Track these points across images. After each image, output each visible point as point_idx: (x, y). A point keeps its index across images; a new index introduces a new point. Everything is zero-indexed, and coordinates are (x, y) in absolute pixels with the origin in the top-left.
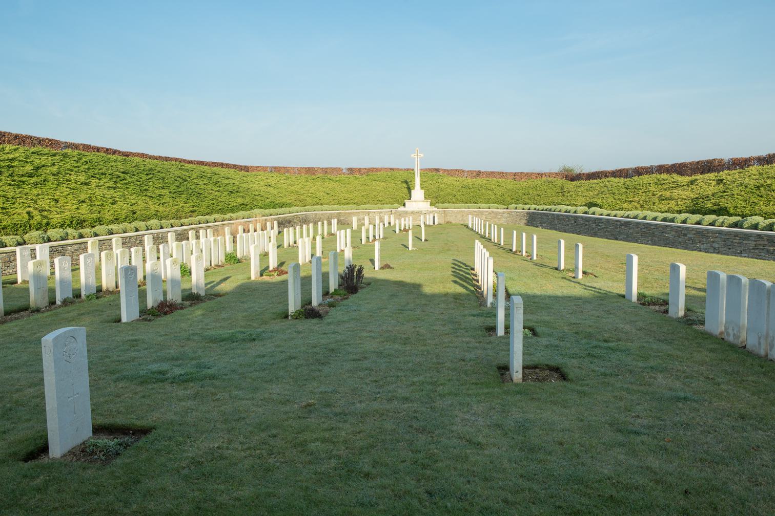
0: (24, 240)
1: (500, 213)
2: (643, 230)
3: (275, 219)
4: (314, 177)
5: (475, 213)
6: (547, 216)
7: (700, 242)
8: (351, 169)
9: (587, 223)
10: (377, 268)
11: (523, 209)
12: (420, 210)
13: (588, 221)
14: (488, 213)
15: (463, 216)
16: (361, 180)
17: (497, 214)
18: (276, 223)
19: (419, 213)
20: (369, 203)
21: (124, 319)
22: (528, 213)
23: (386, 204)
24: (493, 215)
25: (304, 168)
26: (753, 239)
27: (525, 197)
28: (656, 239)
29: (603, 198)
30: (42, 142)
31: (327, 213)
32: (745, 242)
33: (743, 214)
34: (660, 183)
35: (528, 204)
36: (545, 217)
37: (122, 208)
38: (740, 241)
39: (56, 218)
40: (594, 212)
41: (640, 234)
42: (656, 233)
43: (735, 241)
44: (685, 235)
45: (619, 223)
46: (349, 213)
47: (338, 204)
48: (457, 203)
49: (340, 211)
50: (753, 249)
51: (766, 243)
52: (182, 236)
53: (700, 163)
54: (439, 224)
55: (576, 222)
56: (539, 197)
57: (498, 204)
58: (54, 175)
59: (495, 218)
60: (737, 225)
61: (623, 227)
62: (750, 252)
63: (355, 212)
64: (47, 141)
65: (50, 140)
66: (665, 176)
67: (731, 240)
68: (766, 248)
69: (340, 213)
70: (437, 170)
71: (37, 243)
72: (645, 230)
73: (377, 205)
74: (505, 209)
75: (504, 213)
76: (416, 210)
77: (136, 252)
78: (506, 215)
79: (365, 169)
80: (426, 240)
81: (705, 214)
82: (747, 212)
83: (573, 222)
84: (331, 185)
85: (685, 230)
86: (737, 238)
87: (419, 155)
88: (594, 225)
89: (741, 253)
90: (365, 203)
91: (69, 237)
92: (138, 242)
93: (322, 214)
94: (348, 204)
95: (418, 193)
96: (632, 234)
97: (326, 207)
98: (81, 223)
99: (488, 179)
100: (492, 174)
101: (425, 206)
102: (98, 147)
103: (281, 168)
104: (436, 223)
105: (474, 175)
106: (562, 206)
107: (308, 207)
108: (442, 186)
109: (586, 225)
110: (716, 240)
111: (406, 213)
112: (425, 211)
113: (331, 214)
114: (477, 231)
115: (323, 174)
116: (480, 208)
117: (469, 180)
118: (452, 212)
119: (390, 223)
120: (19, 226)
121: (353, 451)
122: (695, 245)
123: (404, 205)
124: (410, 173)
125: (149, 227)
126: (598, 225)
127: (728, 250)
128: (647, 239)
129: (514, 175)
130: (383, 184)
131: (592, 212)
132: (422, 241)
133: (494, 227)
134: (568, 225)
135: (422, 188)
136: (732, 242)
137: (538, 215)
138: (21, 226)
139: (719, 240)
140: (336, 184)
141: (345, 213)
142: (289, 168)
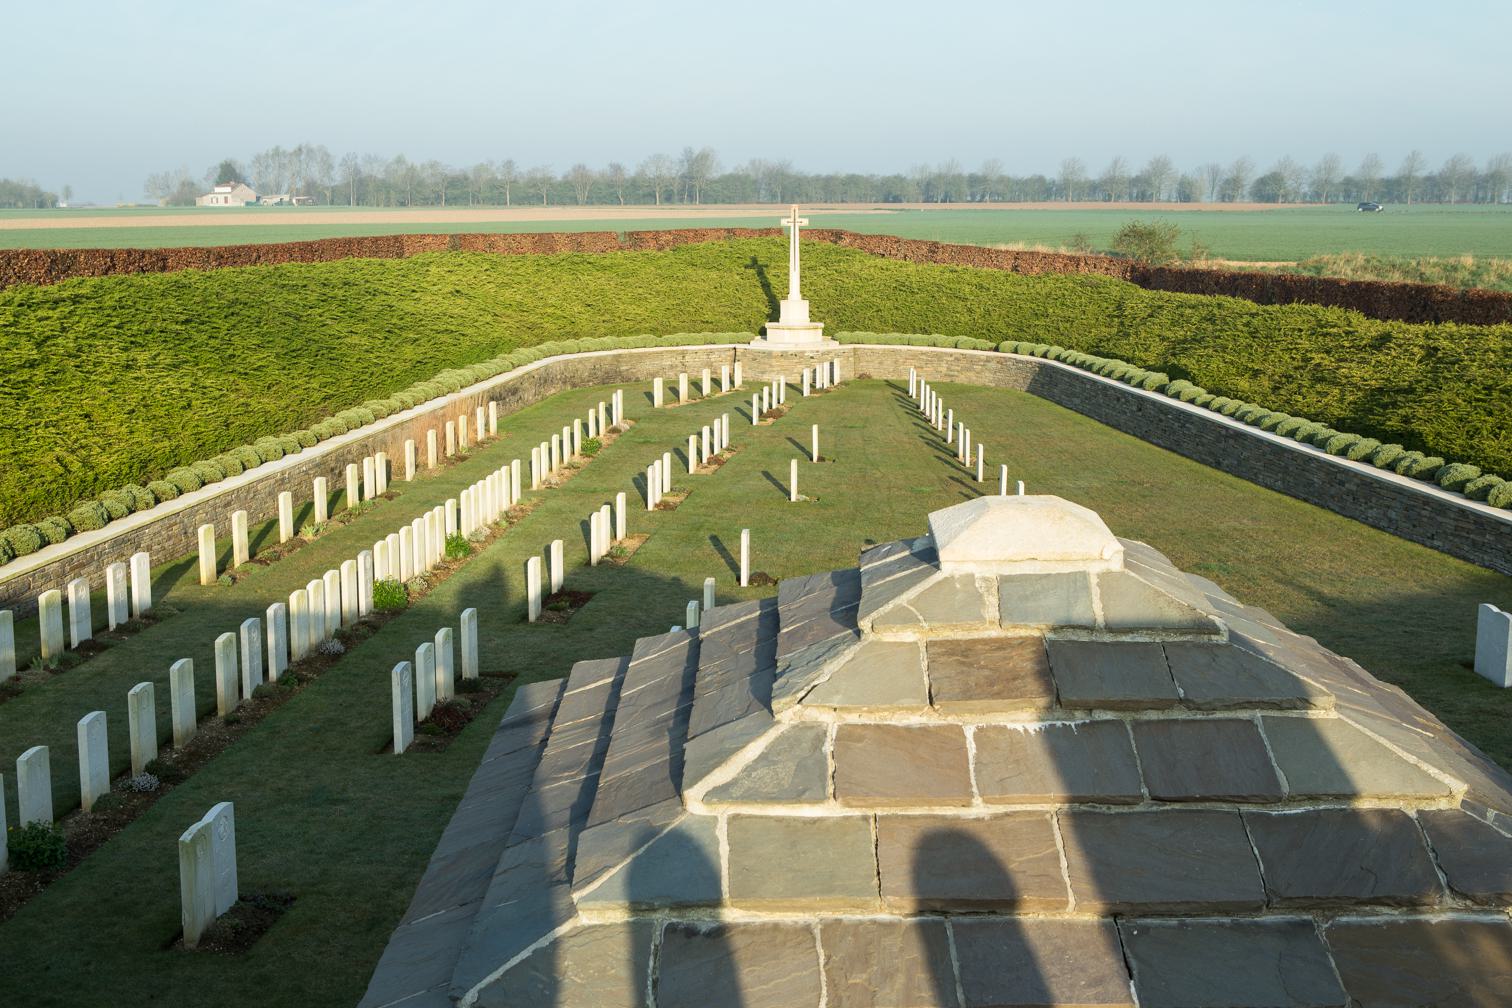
0: (71, 524)
1: (980, 360)
2: (1268, 456)
4: (552, 259)
5: (924, 357)
6: (1082, 382)
7: (1366, 503)
8: (638, 233)
9: (1162, 417)
10: (744, 582)
11: (1032, 354)
12: (799, 349)
13: (1166, 414)
14: (952, 359)
15: (896, 362)
16: (661, 262)
17: (972, 360)
20: (683, 329)
22: (1043, 367)
23: (722, 331)
24: (963, 363)
25: (528, 235)
26: (1452, 516)
27: (1037, 322)
28: (1291, 480)
29: (1202, 356)
30: (13, 261)
32: (1440, 519)
33: (1448, 452)
34: (1319, 329)
35: (1044, 341)
36: (1077, 383)
37: (202, 417)
38: (1433, 515)
40: (1180, 392)
41: (1262, 464)
42: (1291, 469)
43: (1423, 512)
44: (1342, 483)
45: (1224, 432)
47: (612, 334)
48: (883, 331)
49: (620, 351)
50: (1452, 534)
51: (1472, 527)
52: (323, 467)
53: (1408, 289)
54: (844, 383)
55: (1140, 410)
56: (1068, 325)
57: (975, 337)
59: (968, 370)
60: (1433, 476)
61: (1231, 441)
62: (1446, 538)
63: (654, 353)
64: (21, 256)
65: (28, 253)
66: (1333, 314)
67: (1418, 510)
68: (1471, 536)
69: (620, 355)
70: (838, 235)
71: (94, 529)
72: (1272, 457)
73: (701, 335)
74: (990, 349)
76: (792, 349)
78: (993, 365)
79: (670, 232)
80: (821, 459)
81: (1384, 441)
82: (1457, 449)
83: (1135, 408)
84: (593, 281)
85: (1343, 472)
86: (1426, 507)
87: (798, 220)
88: (1176, 424)
89: (1433, 539)
90: (675, 330)
91: (140, 505)
92: (252, 495)
93: (580, 361)
94: (638, 332)
95: (795, 308)
96: (1247, 459)
97: (587, 341)
99: (953, 266)
100: (963, 252)
102: (110, 251)
104: (837, 380)
105: (923, 252)
106: (1119, 362)
107: (548, 343)
108: (850, 283)
109: (1161, 420)
110: (1393, 504)
111: (769, 355)
112: (812, 352)
114: (928, 413)
115: (572, 249)
116: (935, 345)
117: (911, 268)
118: (873, 351)
119: (732, 382)
120: (54, 494)
121: (323, 687)
122: (1357, 507)
123: (763, 333)
124: (775, 244)
125: (263, 459)
126: (1183, 426)
127: (1411, 528)
128: (1274, 476)
129: (1016, 258)
130: (714, 275)
131: (1173, 392)
132: (812, 459)
133: (965, 433)
134: (1126, 413)
135: (804, 297)
136: (1419, 514)
137: (1062, 375)
138: (57, 494)
139: (1398, 505)
140: (602, 279)
141: (631, 355)
142: (495, 235)
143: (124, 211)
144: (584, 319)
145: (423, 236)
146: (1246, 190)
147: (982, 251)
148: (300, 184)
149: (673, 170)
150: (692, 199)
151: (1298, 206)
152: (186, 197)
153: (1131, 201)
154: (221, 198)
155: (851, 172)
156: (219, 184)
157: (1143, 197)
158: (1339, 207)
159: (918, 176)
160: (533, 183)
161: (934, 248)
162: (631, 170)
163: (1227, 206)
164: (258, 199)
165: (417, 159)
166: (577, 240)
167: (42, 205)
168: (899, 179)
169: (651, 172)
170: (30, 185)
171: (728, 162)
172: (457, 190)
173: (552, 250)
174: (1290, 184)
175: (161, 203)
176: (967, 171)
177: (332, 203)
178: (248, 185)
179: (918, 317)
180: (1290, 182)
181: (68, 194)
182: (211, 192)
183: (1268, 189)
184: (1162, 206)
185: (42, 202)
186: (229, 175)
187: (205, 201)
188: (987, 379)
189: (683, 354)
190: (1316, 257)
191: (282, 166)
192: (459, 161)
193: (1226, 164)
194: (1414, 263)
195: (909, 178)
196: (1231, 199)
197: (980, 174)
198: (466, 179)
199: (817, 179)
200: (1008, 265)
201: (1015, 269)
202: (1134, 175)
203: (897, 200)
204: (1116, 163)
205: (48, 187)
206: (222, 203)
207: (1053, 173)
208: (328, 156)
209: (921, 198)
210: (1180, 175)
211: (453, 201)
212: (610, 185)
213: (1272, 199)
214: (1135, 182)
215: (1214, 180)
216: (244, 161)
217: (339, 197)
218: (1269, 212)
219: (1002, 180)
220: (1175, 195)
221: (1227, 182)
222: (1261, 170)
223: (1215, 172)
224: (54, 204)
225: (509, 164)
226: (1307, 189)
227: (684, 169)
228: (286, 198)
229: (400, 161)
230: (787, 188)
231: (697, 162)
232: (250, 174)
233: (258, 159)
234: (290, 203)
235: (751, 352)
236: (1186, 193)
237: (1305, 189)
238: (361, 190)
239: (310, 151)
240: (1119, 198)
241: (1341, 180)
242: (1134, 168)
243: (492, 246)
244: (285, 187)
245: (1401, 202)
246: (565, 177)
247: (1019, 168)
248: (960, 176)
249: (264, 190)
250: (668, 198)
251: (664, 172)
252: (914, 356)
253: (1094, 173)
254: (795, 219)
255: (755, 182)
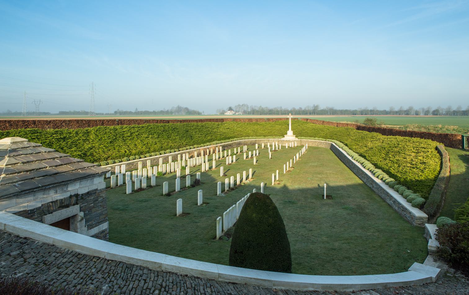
3: (221, 146)
17: (321, 143)
18: (221, 148)
19: (289, 141)
21: (127, 193)
31: (250, 140)
39: (134, 152)
46: (260, 140)
58: (137, 136)
75: (324, 143)
76: (288, 140)
77: (144, 170)
78: (325, 144)
79: (275, 119)
80: (271, 158)
90: (268, 136)
93: (248, 141)
94: (261, 136)
95: (290, 132)
98: (142, 153)
101: (293, 138)
103: (237, 119)
111: (284, 141)
113: (252, 140)
118: (304, 141)
135: (292, 130)
141: (259, 140)
143: (212, 115)
144: (252, 134)
145: (228, 119)
146: (431, 113)
147: (331, 122)
148: (243, 111)
149: (311, 109)
150: (315, 114)
151: (443, 116)
152: (223, 113)
153: (405, 115)
154: (229, 113)
155: (346, 109)
156: (228, 111)
157: (407, 114)
158: (452, 116)
159: (360, 110)
160: (285, 111)
161: (323, 122)
162: (303, 109)
163: (426, 116)
164: (235, 113)
165: (264, 106)
166: (257, 120)
167: (199, 114)
168: (356, 110)
169: (307, 109)
170: (197, 111)
171: (322, 107)
172: (271, 112)
173: (252, 121)
174: (441, 112)
175: (218, 114)
176: (369, 109)
177: (248, 114)
178: (234, 111)
179: (314, 134)
180: (440, 111)
181: (203, 112)
182: (227, 112)
183: (436, 113)
184: (411, 116)
185: (199, 114)
186: (230, 109)
187: (226, 114)
188: (324, 146)
189: (269, 140)
190: (407, 125)
191: (240, 108)
192: (271, 107)
193: (426, 108)
194: (428, 126)
195: (358, 110)
196: (427, 115)
197: (372, 110)
198: (272, 110)
199: (339, 110)
200: (336, 125)
201: (337, 126)
202: (405, 110)
203: (355, 114)
204: (401, 107)
205: (200, 111)
206: (229, 114)
207: (388, 109)
208: (248, 106)
209: (360, 114)
210: (415, 110)
211: (270, 114)
212: (299, 111)
213: (437, 115)
214: (405, 111)
215: (423, 111)
216: (233, 107)
217: (249, 113)
218: (436, 117)
219: (377, 111)
220: (414, 114)
221: (426, 111)
222: (434, 109)
223: (423, 109)
224: (201, 114)
225: (281, 107)
226: (444, 113)
227: (313, 109)
228: (240, 113)
229: (260, 107)
230: (286, 112)
231: (316, 107)
232: (234, 109)
233: (236, 106)
234: (241, 114)
235: (281, 140)
236: (417, 113)
237: (444, 113)
238: (254, 112)
239: (245, 105)
240: (403, 114)
241: (452, 111)
242: (405, 108)
243: (240, 120)
244: (240, 111)
245: (467, 115)
246: (291, 110)
247: (338, 108)
248: (368, 110)
249: (236, 112)
250: (310, 114)
251: (309, 109)
252: (312, 142)
253: (397, 109)
254: (290, 117)
255: (327, 111)
